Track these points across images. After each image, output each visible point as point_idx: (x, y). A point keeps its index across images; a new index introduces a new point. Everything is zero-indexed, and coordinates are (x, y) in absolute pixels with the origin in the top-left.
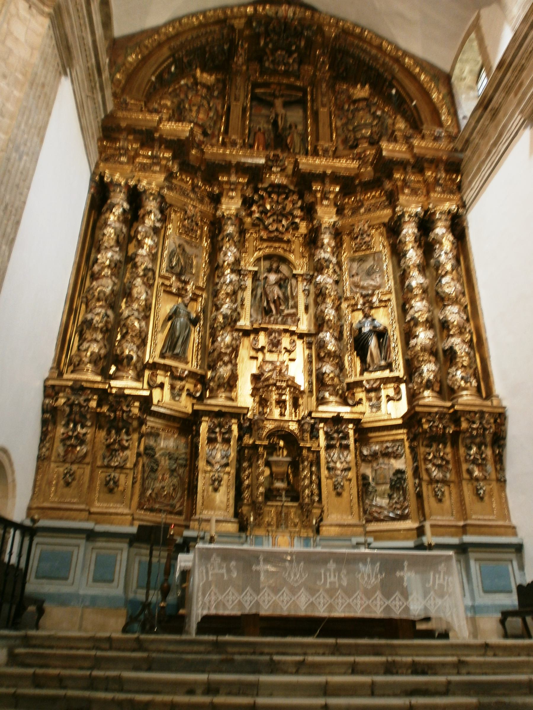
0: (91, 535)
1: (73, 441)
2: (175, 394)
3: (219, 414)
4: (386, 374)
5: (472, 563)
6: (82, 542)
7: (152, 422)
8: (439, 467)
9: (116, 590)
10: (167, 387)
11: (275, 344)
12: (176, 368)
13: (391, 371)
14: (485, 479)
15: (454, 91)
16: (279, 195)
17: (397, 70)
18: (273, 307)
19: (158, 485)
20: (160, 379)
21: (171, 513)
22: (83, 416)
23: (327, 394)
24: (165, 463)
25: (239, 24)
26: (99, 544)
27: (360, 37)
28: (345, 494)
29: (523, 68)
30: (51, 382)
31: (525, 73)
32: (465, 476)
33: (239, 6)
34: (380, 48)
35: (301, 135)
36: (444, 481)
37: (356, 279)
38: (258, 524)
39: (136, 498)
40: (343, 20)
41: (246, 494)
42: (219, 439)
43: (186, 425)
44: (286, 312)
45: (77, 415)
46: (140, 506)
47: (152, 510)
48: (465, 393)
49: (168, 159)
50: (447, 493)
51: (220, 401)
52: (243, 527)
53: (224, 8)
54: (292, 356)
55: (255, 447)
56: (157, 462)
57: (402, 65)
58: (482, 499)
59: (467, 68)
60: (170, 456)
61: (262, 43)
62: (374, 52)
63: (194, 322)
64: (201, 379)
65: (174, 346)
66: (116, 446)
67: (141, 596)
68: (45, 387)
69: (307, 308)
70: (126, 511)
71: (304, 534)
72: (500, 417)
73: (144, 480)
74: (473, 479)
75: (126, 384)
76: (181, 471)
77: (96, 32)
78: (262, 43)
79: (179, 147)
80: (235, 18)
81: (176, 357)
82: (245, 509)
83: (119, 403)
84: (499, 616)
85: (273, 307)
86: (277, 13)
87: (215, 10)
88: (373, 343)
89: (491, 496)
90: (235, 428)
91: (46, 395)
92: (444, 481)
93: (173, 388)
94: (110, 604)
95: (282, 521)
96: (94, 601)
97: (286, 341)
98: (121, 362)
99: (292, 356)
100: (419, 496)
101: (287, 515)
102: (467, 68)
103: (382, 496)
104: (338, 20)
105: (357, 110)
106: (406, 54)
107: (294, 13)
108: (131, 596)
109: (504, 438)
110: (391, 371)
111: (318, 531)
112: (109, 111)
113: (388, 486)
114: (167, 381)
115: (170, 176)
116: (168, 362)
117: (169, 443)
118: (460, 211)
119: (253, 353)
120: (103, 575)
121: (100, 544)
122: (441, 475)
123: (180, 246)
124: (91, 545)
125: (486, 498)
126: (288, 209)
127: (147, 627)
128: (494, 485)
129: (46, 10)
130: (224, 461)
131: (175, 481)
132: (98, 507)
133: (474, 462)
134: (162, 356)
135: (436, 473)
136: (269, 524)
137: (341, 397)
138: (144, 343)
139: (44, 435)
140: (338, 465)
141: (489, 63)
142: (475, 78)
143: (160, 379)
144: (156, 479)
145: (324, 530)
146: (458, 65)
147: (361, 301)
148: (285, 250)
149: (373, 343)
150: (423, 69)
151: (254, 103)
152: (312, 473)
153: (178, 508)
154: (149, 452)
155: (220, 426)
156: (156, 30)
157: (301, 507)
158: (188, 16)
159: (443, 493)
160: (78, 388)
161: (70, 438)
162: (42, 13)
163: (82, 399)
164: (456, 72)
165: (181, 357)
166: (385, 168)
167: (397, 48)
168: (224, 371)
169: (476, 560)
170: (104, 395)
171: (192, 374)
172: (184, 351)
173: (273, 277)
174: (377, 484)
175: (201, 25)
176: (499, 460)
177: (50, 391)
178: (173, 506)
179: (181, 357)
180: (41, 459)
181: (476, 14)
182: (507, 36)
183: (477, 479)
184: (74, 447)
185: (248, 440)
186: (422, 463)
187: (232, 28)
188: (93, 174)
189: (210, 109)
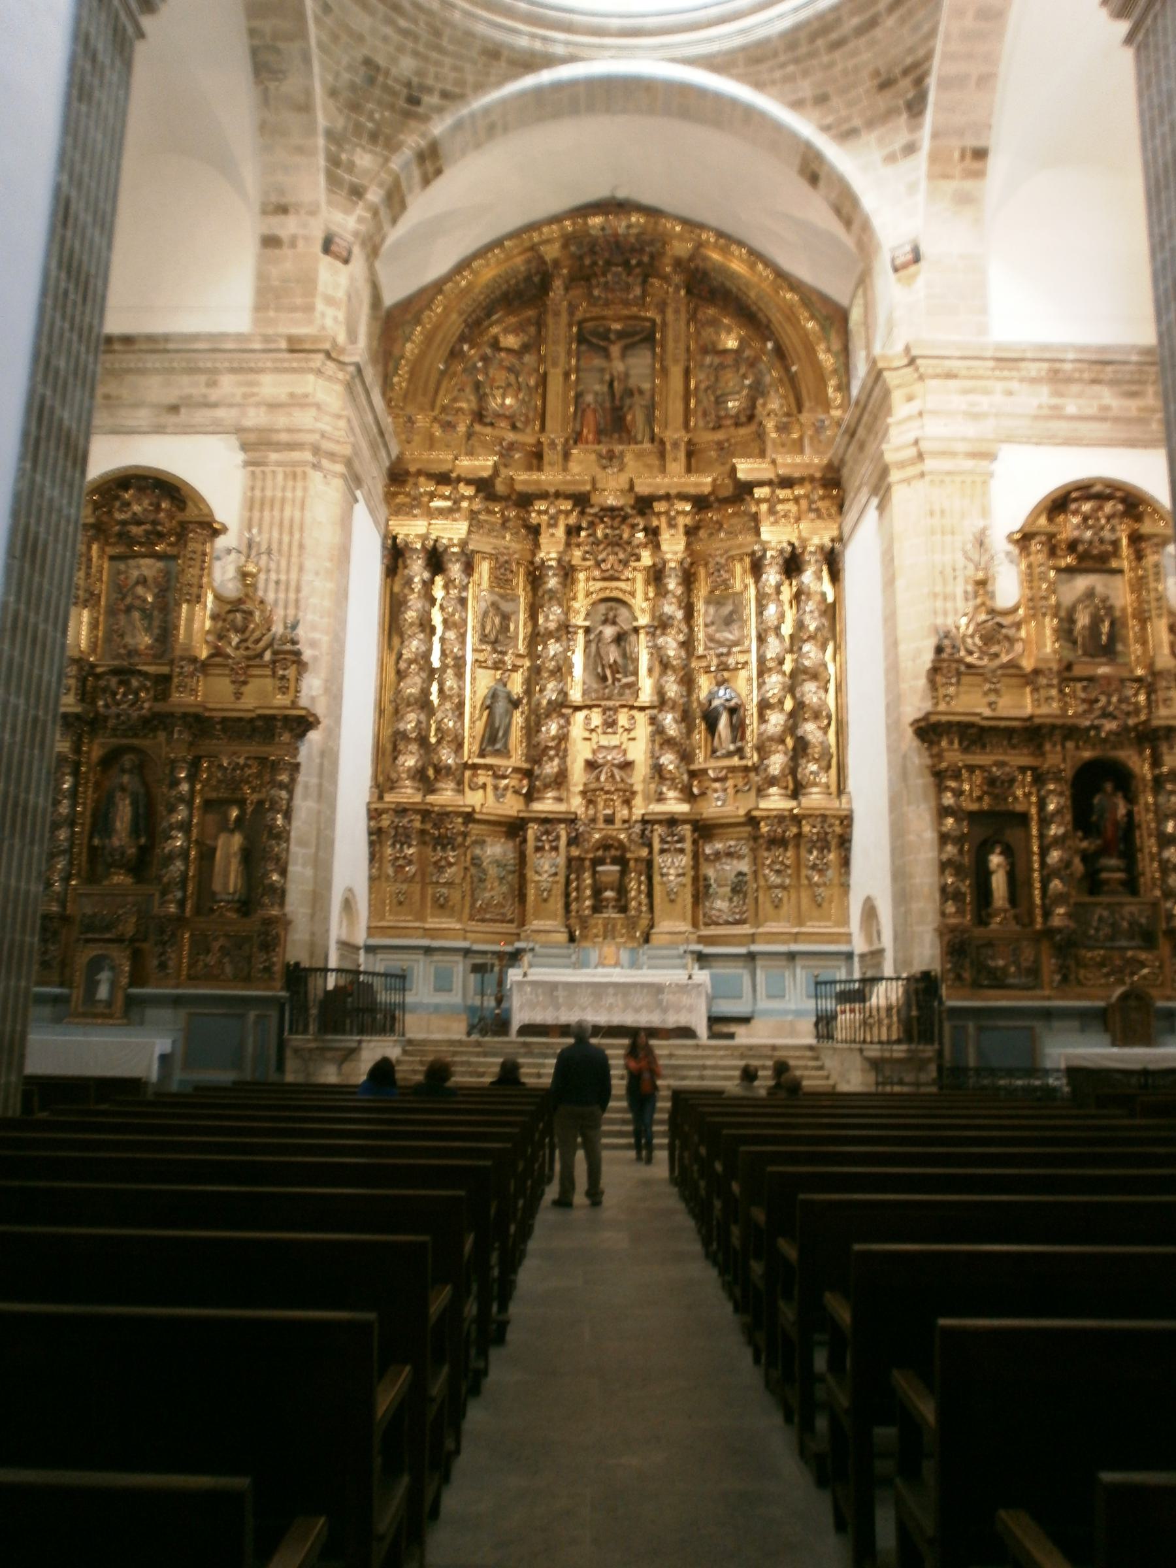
0: (428, 951)
1: (401, 862)
2: (499, 793)
3: (545, 821)
4: (736, 761)
5: (798, 971)
6: (421, 957)
7: (474, 829)
8: (778, 872)
9: (455, 998)
10: (489, 789)
11: (610, 724)
12: (499, 767)
13: (742, 758)
14: (825, 884)
15: (851, 347)
16: (613, 518)
18: (608, 673)
19: (487, 895)
20: (481, 780)
21: (502, 921)
22: (408, 836)
23: (664, 789)
24: (493, 871)
26: (435, 958)
28: (679, 900)
30: (374, 806)
32: (805, 882)
35: (647, 407)
36: (783, 887)
37: (711, 630)
38: (584, 937)
39: (467, 910)
41: (574, 906)
42: (547, 847)
43: (514, 828)
44: (624, 681)
45: (402, 837)
46: (472, 918)
47: (483, 920)
48: (815, 790)
49: (470, 498)
50: (785, 900)
51: (546, 805)
52: (572, 939)
54: (632, 735)
55: (581, 859)
56: (485, 872)
58: (820, 905)
60: (498, 863)
63: (516, 704)
64: (528, 774)
65: (493, 739)
66: (443, 863)
67: (477, 1002)
68: (369, 811)
69: (650, 671)
70: (458, 926)
71: (630, 945)
72: (847, 820)
73: (473, 891)
74: (812, 885)
75: (446, 796)
76: (510, 877)
79: (484, 486)
81: (497, 753)
82: (573, 921)
83: (442, 821)
84: (814, 1019)
85: (608, 673)
88: (724, 720)
89: (831, 902)
90: (563, 834)
91: (370, 818)
92: (783, 887)
93: (496, 788)
94: (452, 1010)
95: (609, 932)
96: (437, 1008)
97: (623, 718)
98: (442, 771)
99: (632, 735)
100: (756, 899)
101: (614, 926)
103: (723, 900)
105: (722, 367)
108: (469, 1002)
109: (850, 841)
110: (742, 758)
111: (647, 940)
112: (394, 456)
113: (728, 889)
114: (490, 781)
115: (473, 515)
116: (488, 761)
117: (496, 849)
118: (837, 545)
119: (587, 735)
120: (442, 984)
121: (437, 957)
122: (779, 881)
123: (493, 604)
124: (429, 959)
125: (825, 905)
126: (626, 536)
127: (484, 1032)
128: (836, 891)
130: (553, 870)
131: (504, 889)
132: (432, 923)
133: (814, 867)
134: (482, 754)
135: (774, 879)
136: (596, 936)
137: (682, 791)
138: (460, 746)
139: (372, 857)
140: (672, 871)
143: (481, 780)
144: (485, 889)
145: (655, 939)
147: (715, 662)
148: (624, 592)
149: (724, 720)
151: (583, 348)
152: (640, 883)
153: (509, 917)
154: (476, 862)
155: (547, 833)
157: (628, 918)
159: (781, 900)
160: (401, 811)
161: (397, 859)
163: (405, 821)
165: (505, 753)
166: (745, 489)
168: (550, 768)
169: (803, 967)
170: (425, 813)
171: (516, 770)
172: (506, 745)
173: (609, 632)
174: (719, 886)
176: (846, 862)
177: (374, 814)
178: (504, 915)
179: (505, 753)
180: (372, 879)
183: (817, 885)
184: (402, 867)
185: (575, 852)
188: (385, 537)
189: (519, 389)
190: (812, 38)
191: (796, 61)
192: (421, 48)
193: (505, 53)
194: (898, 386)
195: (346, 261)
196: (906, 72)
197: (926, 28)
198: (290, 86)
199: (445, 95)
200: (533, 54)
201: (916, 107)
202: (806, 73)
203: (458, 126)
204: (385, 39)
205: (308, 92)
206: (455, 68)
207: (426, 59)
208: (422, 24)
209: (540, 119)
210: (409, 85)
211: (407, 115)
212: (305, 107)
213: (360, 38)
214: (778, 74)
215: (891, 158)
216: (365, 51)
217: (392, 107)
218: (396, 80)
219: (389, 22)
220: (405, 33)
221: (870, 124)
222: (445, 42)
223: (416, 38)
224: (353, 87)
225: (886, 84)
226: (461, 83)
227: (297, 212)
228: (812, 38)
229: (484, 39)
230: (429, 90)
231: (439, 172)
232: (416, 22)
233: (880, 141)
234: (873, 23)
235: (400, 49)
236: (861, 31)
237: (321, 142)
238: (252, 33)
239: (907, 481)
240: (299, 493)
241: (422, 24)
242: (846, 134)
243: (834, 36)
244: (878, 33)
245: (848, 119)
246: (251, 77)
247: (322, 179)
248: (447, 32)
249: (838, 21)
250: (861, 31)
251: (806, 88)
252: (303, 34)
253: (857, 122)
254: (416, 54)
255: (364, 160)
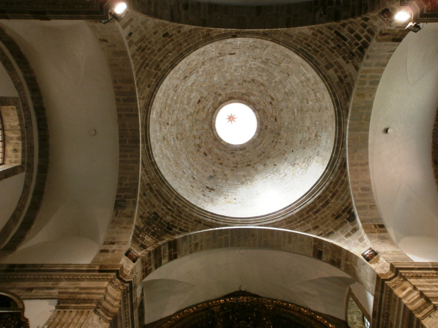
17: (314, 323)
25: (216, 309)
27: (287, 307)
29: (388, 315)
31: (390, 318)
33: (216, 300)
34: (300, 312)
40: (275, 300)
53: (207, 302)
57: (316, 320)
59: (355, 317)
61: (231, 317)
62: (297, 314)
77: (135, 326)
78: (231, 317)
80: (214, 306)
86: (237, 301)
87: (202, 303)
102: (355, 317)
104: (272, 300)
106: (317, 313)
107: (247, 300)
129: (109, 318)
141: (367, 312)
142: (361, 322)
146: (349, 316)
150: (329, 321)
156: (169, 318)
158: (187, 308)
162: (106, 321)
164: (349, 319)
167: (310, 311)
175: (195, 312)
181: (348, 288)
182: (371, 299)
186: (380, 11)
187: (213, 311)
190: (308, 212)
191: (304, 220)
192: (174, 215)
193: (203, 222)
194: (395, 287)
195: (134, 261)
196: (343, 212)
197: (346, 198)
198: (127, 211)
199: (180, 229)
200: (212, 223)
201: (352, 218)
202: (308, 222)
203: (185, 238)
204: (162, 209)
205: (133, 212)
206: (185, 223)
207: (176, 219)
208: (175, 209)
209: (214, 247)
210: (168, 224)
211: (167, 232)
212: (131, 216)
213: (154, 206)
214: (298, 224)
215: (348, 235)
216: (155, 210)
217: (161, 228)
218: (164, 221)
219: (164, 205)
220: (170, 210)
221: (336, 229)
222: (182, 216)
223: (173, 212)
224: (148, 218)
225: (338, 217)
226: (188, 228)
227: (118, 244)
228: (308, 212)
229: (196, 217)
230: (176, 227)
231: (175, 257)
232: (174, 208)
233: (342, 232)
234: (327, 202)
235: (167, 213)
236: (323, 206)
237: (133, 228)
238: (117, 196)
239: (428, 315)
240: (82, 320)
241: (175, 209)
242: (329, 234)
243: (315, 210)
244: (330, 205)
245: (328, 230)
246: (114, 206)
247: (131, 237)
248: (184, 213)
249: (315, 206)
250: (323, 206)
251: (309, 226)
252: (135, 197)
253: (331, 230)
254: (172, 216)
255: (148, 239)
